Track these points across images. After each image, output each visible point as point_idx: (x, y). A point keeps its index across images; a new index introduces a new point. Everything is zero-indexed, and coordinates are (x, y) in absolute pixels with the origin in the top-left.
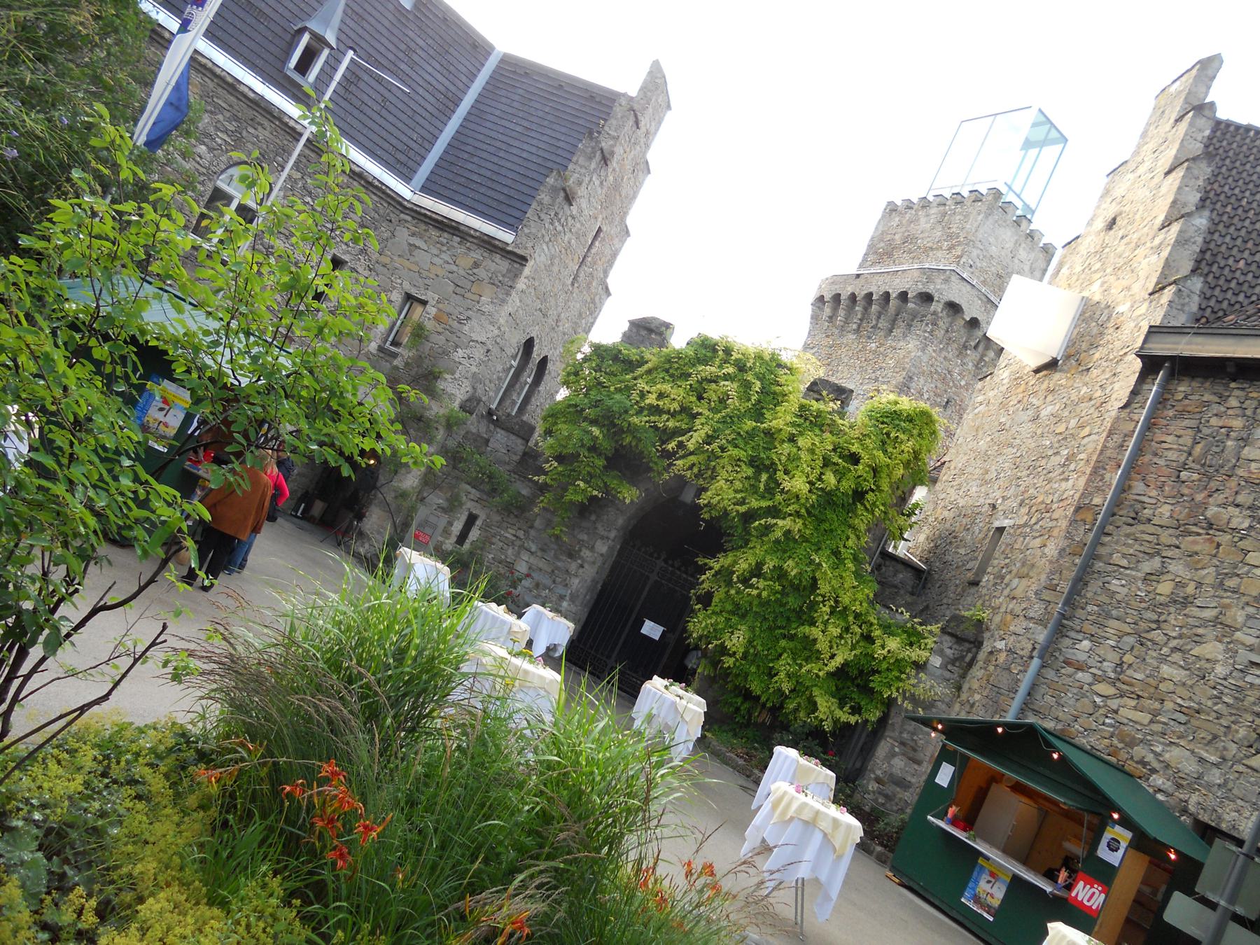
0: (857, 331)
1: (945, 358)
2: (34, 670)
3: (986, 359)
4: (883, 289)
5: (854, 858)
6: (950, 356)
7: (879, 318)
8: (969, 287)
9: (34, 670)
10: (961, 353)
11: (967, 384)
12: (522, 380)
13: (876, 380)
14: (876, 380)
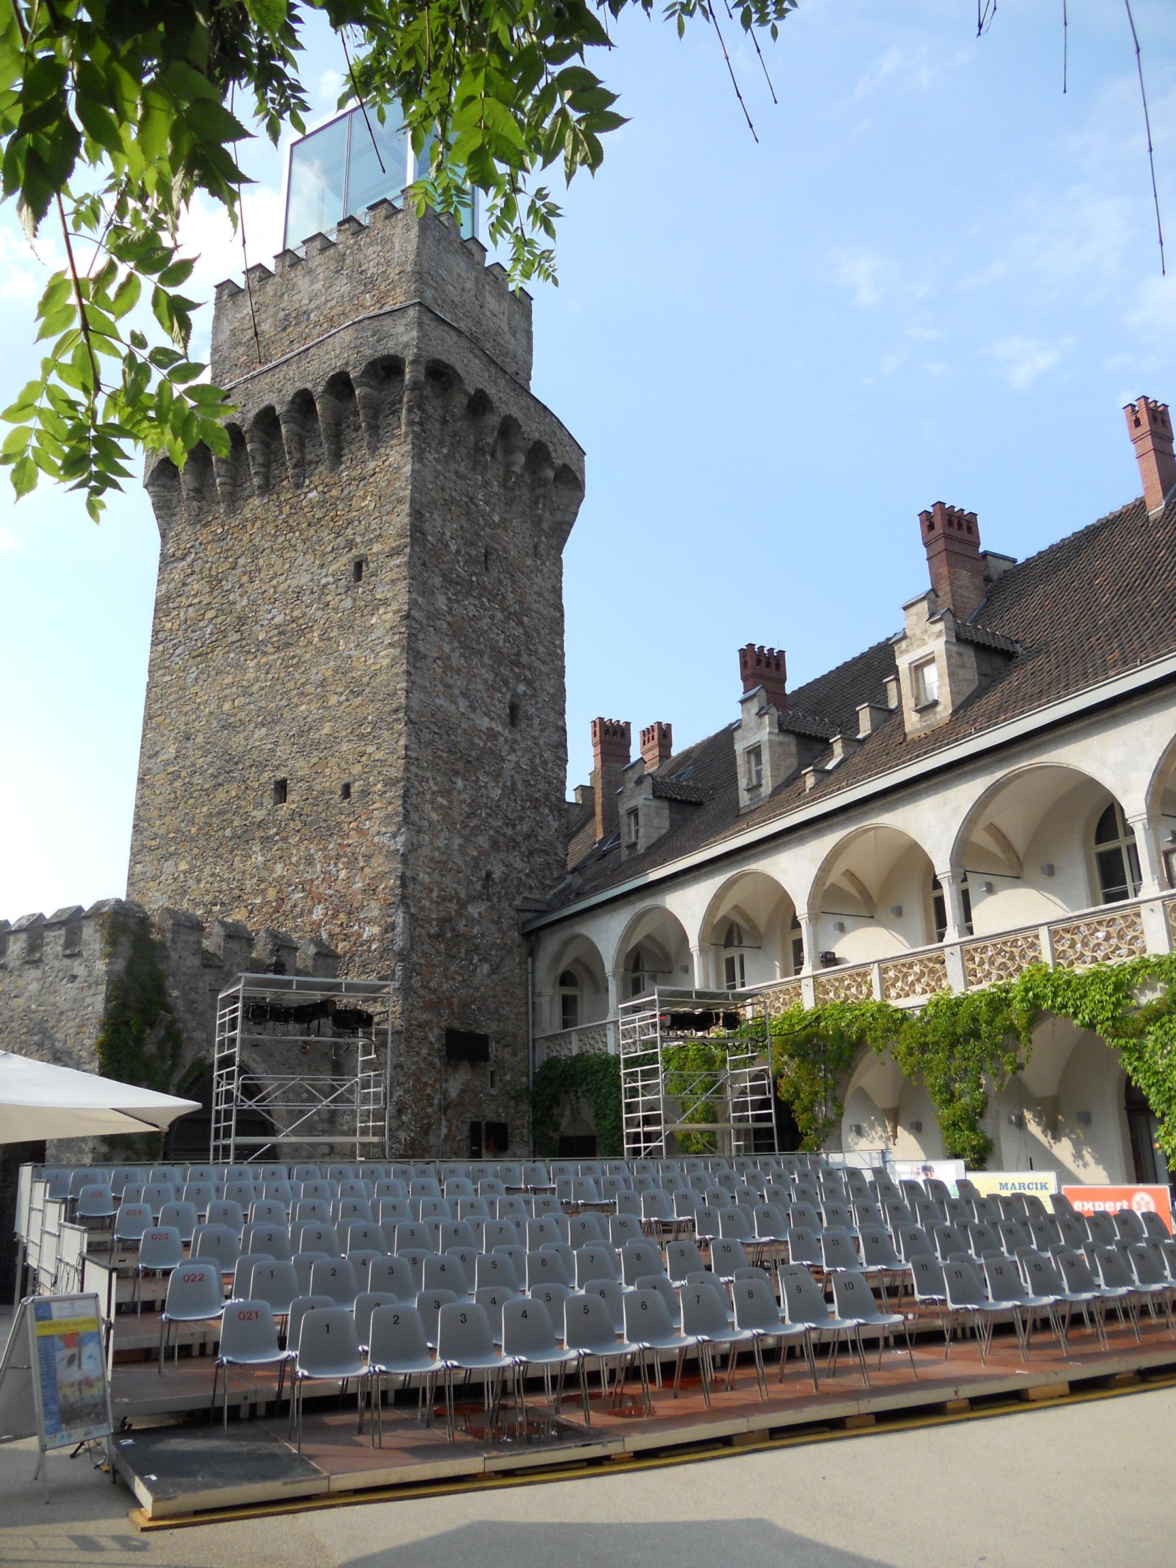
0: (266, 488)
1: (457, 473)
2: (529, 911)
3: (517, 469)
4: (290, 391)
5: (1000, 1168)
6: (462, 469)
7: (302, 446)
8: (453, 334)
9: (529, 911)
10: (476, 462)
11: (503, 519)
12: (672, 1412)
13: (351, 544)
14: (351, 544)
